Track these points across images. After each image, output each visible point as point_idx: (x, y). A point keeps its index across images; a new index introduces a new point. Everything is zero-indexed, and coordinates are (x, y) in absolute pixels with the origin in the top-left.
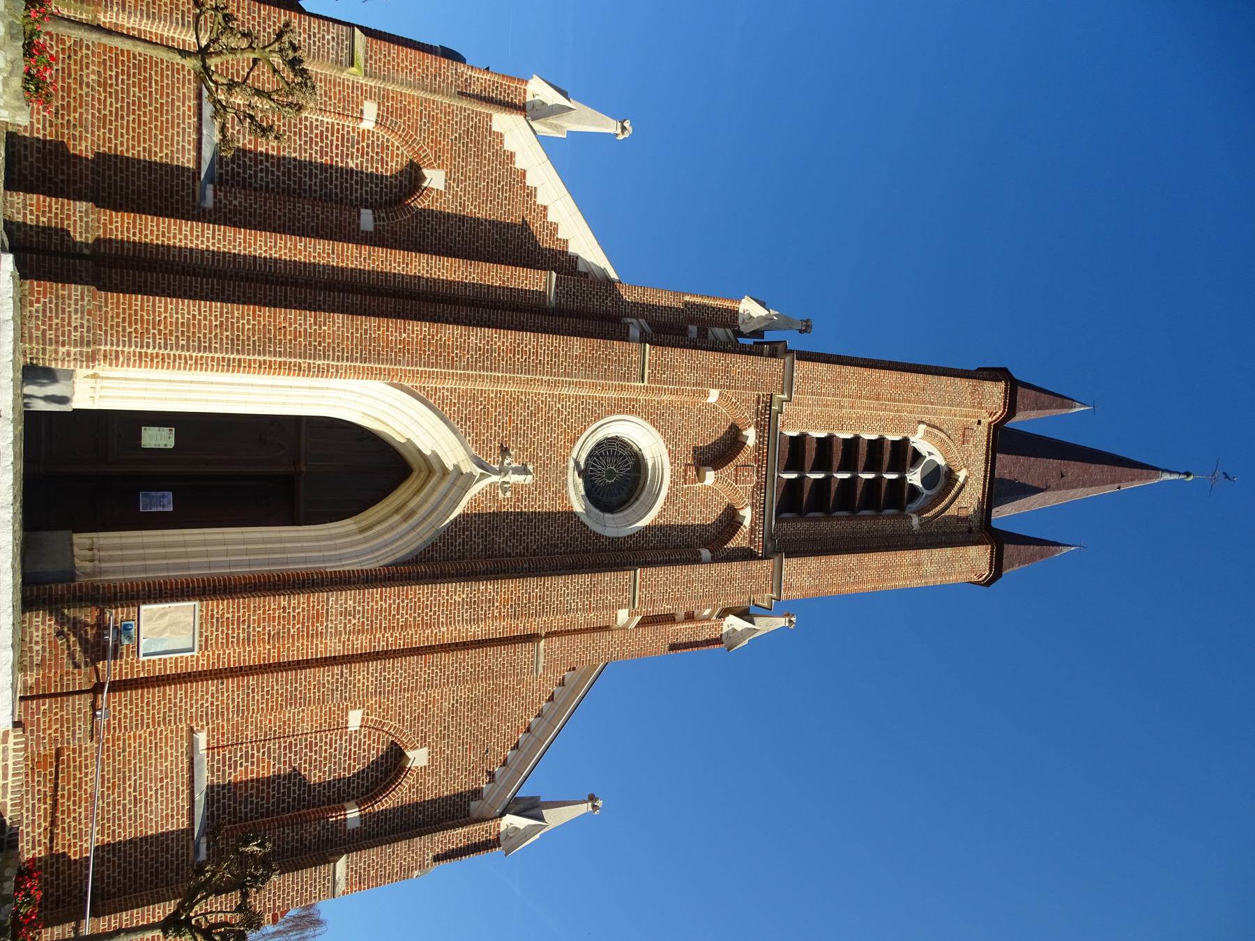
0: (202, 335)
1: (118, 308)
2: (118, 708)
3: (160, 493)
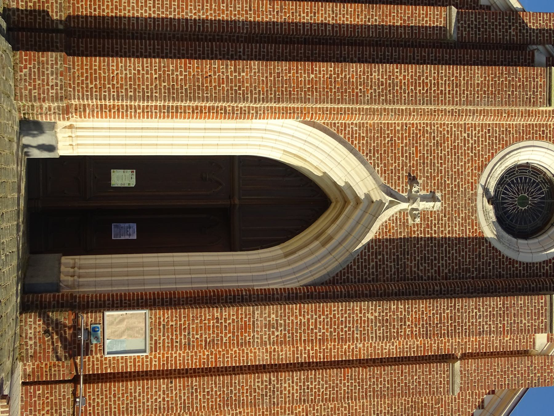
0: (145, 87)
1: (82, 69)
2: (92, 397)
3: (127, 225)
